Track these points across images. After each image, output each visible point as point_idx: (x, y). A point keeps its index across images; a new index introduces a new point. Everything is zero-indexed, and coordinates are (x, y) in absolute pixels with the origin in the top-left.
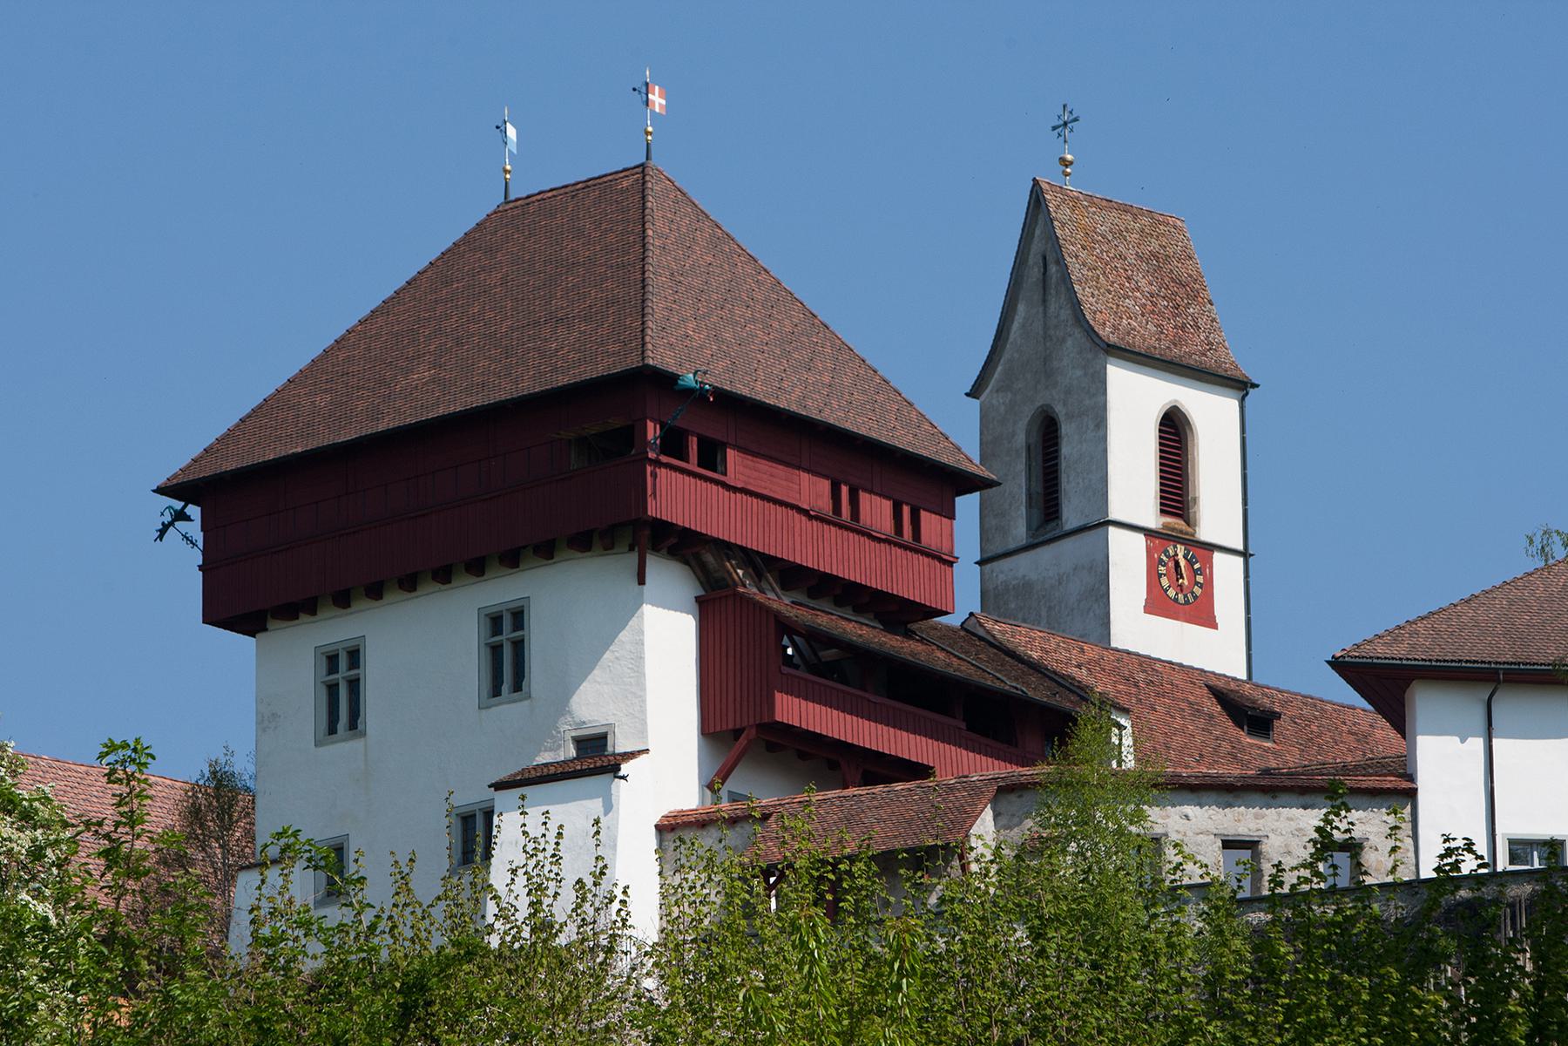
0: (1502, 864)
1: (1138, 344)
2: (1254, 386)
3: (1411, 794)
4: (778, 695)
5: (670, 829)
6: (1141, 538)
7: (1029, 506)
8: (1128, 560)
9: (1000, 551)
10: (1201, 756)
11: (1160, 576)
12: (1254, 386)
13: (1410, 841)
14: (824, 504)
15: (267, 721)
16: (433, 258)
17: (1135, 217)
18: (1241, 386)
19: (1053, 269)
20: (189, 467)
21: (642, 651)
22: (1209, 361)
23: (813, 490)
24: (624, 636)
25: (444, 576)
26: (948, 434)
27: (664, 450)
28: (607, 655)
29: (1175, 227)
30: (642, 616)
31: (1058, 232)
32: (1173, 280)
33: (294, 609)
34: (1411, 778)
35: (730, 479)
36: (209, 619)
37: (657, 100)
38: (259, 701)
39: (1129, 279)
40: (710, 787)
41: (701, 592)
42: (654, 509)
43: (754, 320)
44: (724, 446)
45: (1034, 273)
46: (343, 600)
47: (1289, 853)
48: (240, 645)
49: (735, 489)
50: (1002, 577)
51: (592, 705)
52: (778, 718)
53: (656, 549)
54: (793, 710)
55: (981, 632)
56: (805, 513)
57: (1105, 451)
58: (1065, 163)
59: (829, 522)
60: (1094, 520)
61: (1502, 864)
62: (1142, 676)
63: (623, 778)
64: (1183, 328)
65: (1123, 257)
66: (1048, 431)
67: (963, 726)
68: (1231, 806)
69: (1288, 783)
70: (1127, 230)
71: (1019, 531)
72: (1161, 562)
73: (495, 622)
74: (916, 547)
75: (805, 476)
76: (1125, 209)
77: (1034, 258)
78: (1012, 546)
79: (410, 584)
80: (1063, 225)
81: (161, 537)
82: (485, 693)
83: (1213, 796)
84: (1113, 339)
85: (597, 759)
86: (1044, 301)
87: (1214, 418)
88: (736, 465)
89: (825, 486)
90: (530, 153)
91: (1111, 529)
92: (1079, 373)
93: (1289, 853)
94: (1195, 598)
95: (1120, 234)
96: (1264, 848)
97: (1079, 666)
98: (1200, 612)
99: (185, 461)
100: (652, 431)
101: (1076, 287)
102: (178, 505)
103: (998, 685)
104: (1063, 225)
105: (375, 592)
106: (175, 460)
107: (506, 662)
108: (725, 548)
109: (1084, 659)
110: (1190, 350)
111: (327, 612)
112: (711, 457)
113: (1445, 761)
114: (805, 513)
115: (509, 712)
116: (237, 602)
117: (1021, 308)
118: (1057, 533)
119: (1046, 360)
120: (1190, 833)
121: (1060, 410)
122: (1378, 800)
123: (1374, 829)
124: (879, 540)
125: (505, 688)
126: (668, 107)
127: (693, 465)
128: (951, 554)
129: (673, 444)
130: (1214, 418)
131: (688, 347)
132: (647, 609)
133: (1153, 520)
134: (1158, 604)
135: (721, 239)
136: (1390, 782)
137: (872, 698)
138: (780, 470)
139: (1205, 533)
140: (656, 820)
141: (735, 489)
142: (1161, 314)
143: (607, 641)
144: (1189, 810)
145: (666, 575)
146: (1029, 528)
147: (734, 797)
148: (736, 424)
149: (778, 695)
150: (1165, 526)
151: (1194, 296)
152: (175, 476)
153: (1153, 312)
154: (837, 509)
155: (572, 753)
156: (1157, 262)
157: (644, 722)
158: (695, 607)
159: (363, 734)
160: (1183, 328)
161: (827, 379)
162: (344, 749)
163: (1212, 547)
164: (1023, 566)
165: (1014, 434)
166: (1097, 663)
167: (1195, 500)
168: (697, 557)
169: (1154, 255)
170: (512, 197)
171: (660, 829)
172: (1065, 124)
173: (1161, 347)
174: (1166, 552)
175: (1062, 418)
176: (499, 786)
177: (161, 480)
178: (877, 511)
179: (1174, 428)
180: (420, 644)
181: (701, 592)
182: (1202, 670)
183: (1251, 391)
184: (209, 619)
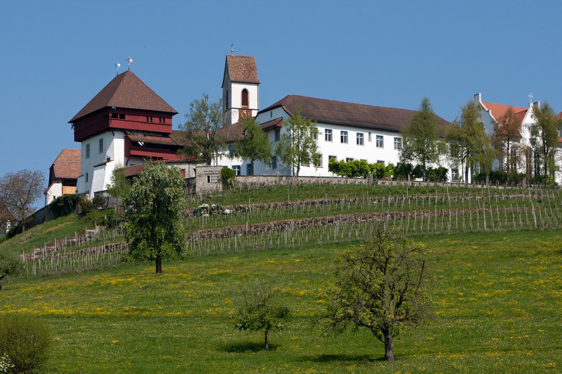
1: (238, 80)
18: (257, 84)
23: (143, 119)
27: (113, 117)
36: (75, 141)
40: (126, 164)
42: (110, 126)
48: (79, 143)
54: (133, 152)
76: (243, 57)
79: (102, 133)
87: (253, 90)
88: (127, 117)
89: (146, 118)
106: (70, 119)
107: (102, 149)
110: (250, 80)
112: (122, 117)
116: (78, 138)
129: (115, 116)
130: (253, 90)
132: (115, 140)
133: (240, 106)
138: (136, 117)
139: (250, 107)
147: (131, 165)
148: (122, 113)
156: (247, 65)
173: (242, 79)
178: (156, 120)
179: (245, 93)
180: (94, 142)
182: (328, 101)
184: (75, 141)
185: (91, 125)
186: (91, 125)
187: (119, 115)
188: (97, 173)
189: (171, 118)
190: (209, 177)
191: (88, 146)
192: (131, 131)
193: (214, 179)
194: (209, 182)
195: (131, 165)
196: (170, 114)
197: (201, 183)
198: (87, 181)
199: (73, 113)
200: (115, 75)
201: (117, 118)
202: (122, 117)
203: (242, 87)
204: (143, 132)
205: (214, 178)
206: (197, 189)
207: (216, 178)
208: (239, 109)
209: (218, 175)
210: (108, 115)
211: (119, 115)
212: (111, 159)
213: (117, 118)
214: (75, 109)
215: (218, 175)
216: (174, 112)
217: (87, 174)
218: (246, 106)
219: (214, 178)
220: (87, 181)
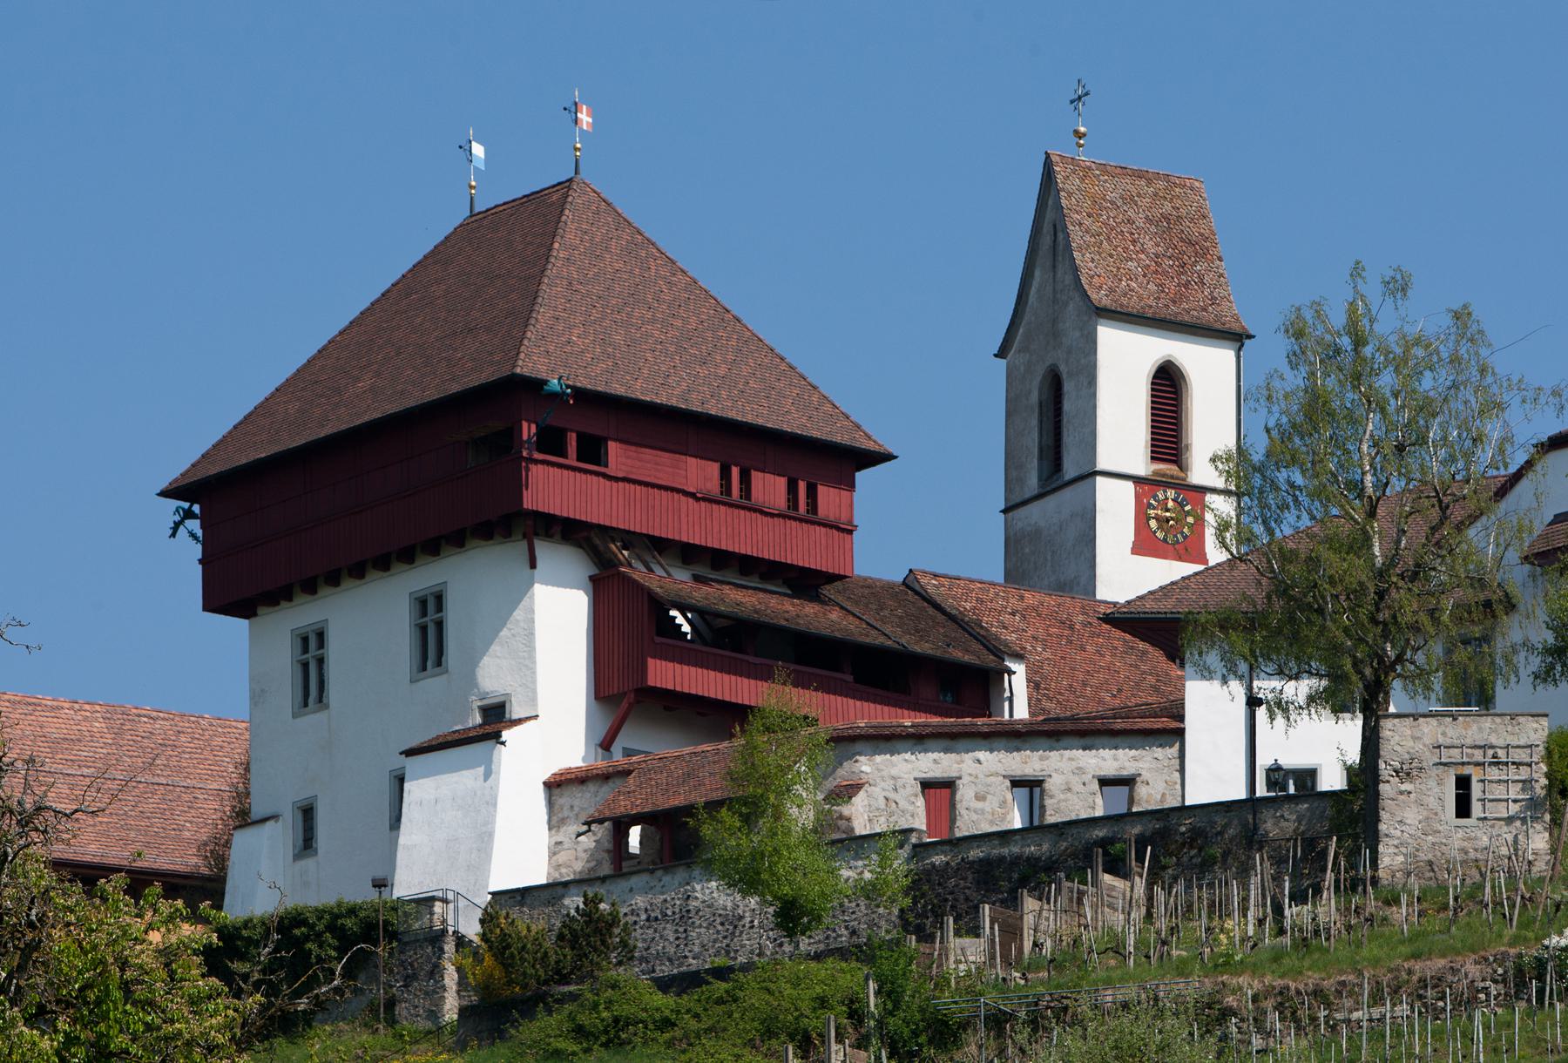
0: (1261, 791)
1: (1133, 304)
2: (1250, 337)
3: (1180, 733)
4: (651, 661)
6: (1129, 486)
7: (1041, 458)
8: (1115, 509)
9: (1018, 500)
10: (1119, 690)
11: (1149, 518)
12: (1250, 337)
13: (1177, 775)
14: (713, 485)
15: (258, 697)
16: (404, 271)
17: (1149, 182)
18: (1236, 337)
19: (1061, 236)
20: (188, 471)
21: (533, 628)
22: (1208, 318)
23: (701, 473)
24: (518, 614)
25: (383, 564)
26: (848, 413)
28: (504, 633)
29: (1192, 189)
30: (532, 598)
31: (1064, 202)
32: (1182, 240)
33: (277, 596)
34: (1181, 718)
35: (610, 471)
36: (206, 608)
37: (584, 118)
38: (252, 679)
39: (1134, 242)
40: (606, 745)
41: (594, 571)
43: (654, 320)
44: (606, 440)
45: (1047, 240)
46: (310, 588)
47: (1069, 789)
48: (236, 628)
49: (617, 479)
50: (1020, 525)
51: (493, 676)
52: (651, 683)
53: (537, 534)
54: (664, 674)
55: (917, 587)
56: (693, 495)
57: (1095, 407)
58: (1079, 135)
59: (718, 502)
60: (1086, 470)
61: (1261, 791)
62: (1081, 618)
63: (503, 743)
64: (1187, 285)
65: (1130, 221)
66: (1055, 385)
67: (850, 678)
68: (1018, 750)
69: (1069, 727)
70: (1139, 195)
71: (1032, 483)
72: (1150, 506)
74: (812, 518)
75: (692, 461)
76: (1140, 174)
77: (1047, 228)
78: (1027, 495)
79: (358, 572)
80: (1070, 194)
81: (173, 535)
82: (415, 669)
83: (1003, 742)
84: (1106, 302)
86: (1054, 267)
87: (1210, 372)
88: (618, 455)
90: (489, 170)
91: (1099, 479)
92: (1077, 334)
93: (1069, 789)
94: (1185, 537)
95: (1130, 200)
96: (1047, 786)
97: (1013, 614)
99: (185, 465)
100: (528, 430)
101: (1076, 254)
102: (186, 505)
103: (881, 640)
104: (1070, 194)
105: (334, 580)
106: (176, 466)
107: (431, 643)
108: (607, 532)
109: (1020, 606)
110: (1188, 309)
111: (300, 598)
112: (592, 452)
113: (1211, 705)
114: (693, 495)
115: (433, 684)
117: (1037, 273)
118: (1059, 483)
119: (1055, 321)
120: (981, 776)
121: (1063, 369)
122: (1151, 739)
123: (1146, 765)
124: (772, 515)
125: (429, 664)
126: (594, 125)
127: (572, 460)
128: (850, 522)
129: (551, 442)
130: (1210, 372)
131: (563, 349)
134: (1145, 545)
135: (640, 245)
136: (1165, 723)
137: (751, 659)
138: (666, 457)
140: (546, 776)
141: (617, 479)
142: (1165, 273)
143: (502, 619)
144: (982, 755)
145: (551, 555)
146: (1040, 479)
147: (628, 753)
148: (599, 422)
149: (651, 661)
150: (1155, 473)
151: (1203, 254)
152: (176, 480)
153: (1156, 272)
154: (729, 492)
155: (479, 720)
156: (1166, 224)
157: (534, 691)
158: (590, 586)
159: (327, 707)
160: (1187, 285)
161: (721, 372)
162: (314, 719)
163: (1204, 490)
164: (1034, 514)
165: (1030, 392)
166: (1035, 609)
167: (1187, 446)
168: (588, 540)
169: (1166, 218)
170: (477, 210)
171: (548, 785)
172: (1080, 98)
174: (1155, 497)
175: (1064, 376)
176: (410, 753)
177: (163, 484)
178: (770, 488)
179: (1168, 385)
180: (365, 621)
181: (594, 571)
183: (1247, 342)
184: (206, 608)
185: (339, 503)
186: (339, 503)
187: (572, 439)
188: (431, 794)
189: (851, 485)
190: (1463, 783)
191: (312, 644)
192: (629, 539)
193: (1500, 794)
194: (1463, 809)
195: (628, 753)
196: (848, 460)
197: (1412, 816)
198: (307, 843)
199: (195, 432)
201: (563, 453)
202: (592, 452)
203: (1152, 348)
204: (689, 554)
205: (1498, 791)
206: (1390, 858)
207: (1514, 791)
208: (1137, 480)
209: (1524, 773)
210: (512, 433)
211: (572, 439)
212: (516, 711)
213: (563, 453)
214: (213, 398)
215: (1524, 773)
216: (870, 446)
217: (308, 813)
218: (1172, 469)
219: (1498, 791)
220: (307, 843)
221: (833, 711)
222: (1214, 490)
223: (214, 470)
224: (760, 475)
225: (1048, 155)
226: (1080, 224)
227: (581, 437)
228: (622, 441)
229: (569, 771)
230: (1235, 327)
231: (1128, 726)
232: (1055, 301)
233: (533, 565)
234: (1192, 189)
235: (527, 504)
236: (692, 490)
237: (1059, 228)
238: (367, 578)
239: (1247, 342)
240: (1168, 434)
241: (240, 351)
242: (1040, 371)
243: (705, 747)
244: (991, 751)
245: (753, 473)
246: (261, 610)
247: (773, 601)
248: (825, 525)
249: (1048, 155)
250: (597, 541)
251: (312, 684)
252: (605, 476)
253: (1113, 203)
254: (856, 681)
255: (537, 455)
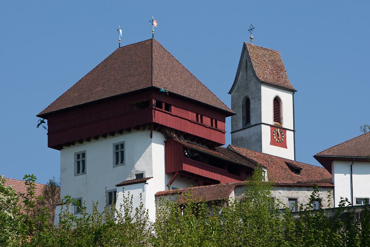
1: (269, 81)
5: (158, 196)
6: (269, 127)
10: (283, 178)
11: (274, 136)
14: (194, 119)
18: (293, 91)
19: (248, 63)
21: (151, 154)
22: (285, 85)
23: (192, 116)
25: (105, 136)
27: (157, 106)
29: (277, 54)
34: (333, 184)
35: (172, 113)
36: (50, 146)
37: (155, 23)
38: (61, 166)
39: (266, 66)
41: (165, 140)
43: (178, 76)
44: (171, 105)
45: (244, 65)
46: (81, 142)
49: (173, 116)
51: (140, 166)
52: (184, 170)
53: (155, 130)
55: (232, 149)
57: (261, 106)
58: (251, 38)
59: (196, 123)
64: (279, 77)
66: (247, 102)
68: (290, 190)
69: (304, 185)
71: (241, 126)
73: (117, 147)
76: (266, 49)
77: (244, 61)
78: (239, 129)
79: (97, 138)
80: (251, 53)
81: (38, 127)
84: (263, 80)
85: (141, 179)
87: (286, 98)
88: (174, 110)
89: (195, 115)
90: (125, 37)
91: (262, 125)
92: (255, 88)
94: (282, 141)
95: (264, 55)
96: (298, 200)
97: (255, 157)
98: (283, 145)
100: (154, 102)
102: (42, 119)
103: (235, 162)
104: (251, 53)
105: (89, 140)
106: (42, 108)
107: (120, 157)
108: (171, 129)
109: (256, 156)
110: (281, 82)
112: (168, 108)
113: (341, 180)
115: (120, 168)
116: (56, 142)
117: (241, 73)
118: (249, 126)
119: (247, 85)
120: (281, 197)
121: (250, 97)
124: (208, 128)
125: (119, 162)
127: (163, 110)
129: (159, 105)
130: (286, 98)
131: (163, 81)
132: (153, 144)
134: (273, 143)
136: (328, 185)
138: (184, 111)
139: (284, 126)
140: (155, 194)
141: (173, 116)
144: (280, 191)
145: (157, 136)
146: (243, 125)
147: (173, 188)
149: (183, 164)
150: (275, 124)
151: (282, 70)
152: (41, 112)
153: (272, 74)
155: (135, 178)
156: (273, 62)
157: (152, 170)
161: (195, 90)
162: (81, 177)
163: (286, 129)
165: (239, 102)
166: (259, 156)
167: (282, 118)
168: (164, 131)
171: (156, 196)
174: (275, 130)
176: (118, 186)
177: (38, 113)
179: (277, 101)
180: (99, 152)
181: (165, 140)
183: (295, 92)
184: (50, 146)
185: (85, 120)
187: (164, 104)
199: (47, 99)
200: (114, 48)
208: (271, 126)
211: (164, 104)
212: (146, 176)
218: (278, 124)
221: (224, 180)
222: (288, 130)
223: (55, 110)
224: (205, 117)
225: (244, 43)
226: (254, 61)
227: (165, 104)
228: (175, 106)
229: (161, 192)
230: (292, 88)
231: (323, 185)
232: (247, 80)
233: (151, 137)
234: (277, 54)
235: (154, 121)
236: (190, 120)
237: (248, 60)
238: (99, 140)
239: (295, 92)
240: (277, 116)
241: (60, 78)
242: (242, 97)
243: (196, 187)
244: (284, 190)
245: (203, 116)
246: (64, 147)
247: (204, 149)
248: (219, 131)
249: (244, 43)
250: (167, 132)
251: (81, 166)
252: (171, 115)
253: (260, 56)
254: (229, 172)
255: (157, 108)
